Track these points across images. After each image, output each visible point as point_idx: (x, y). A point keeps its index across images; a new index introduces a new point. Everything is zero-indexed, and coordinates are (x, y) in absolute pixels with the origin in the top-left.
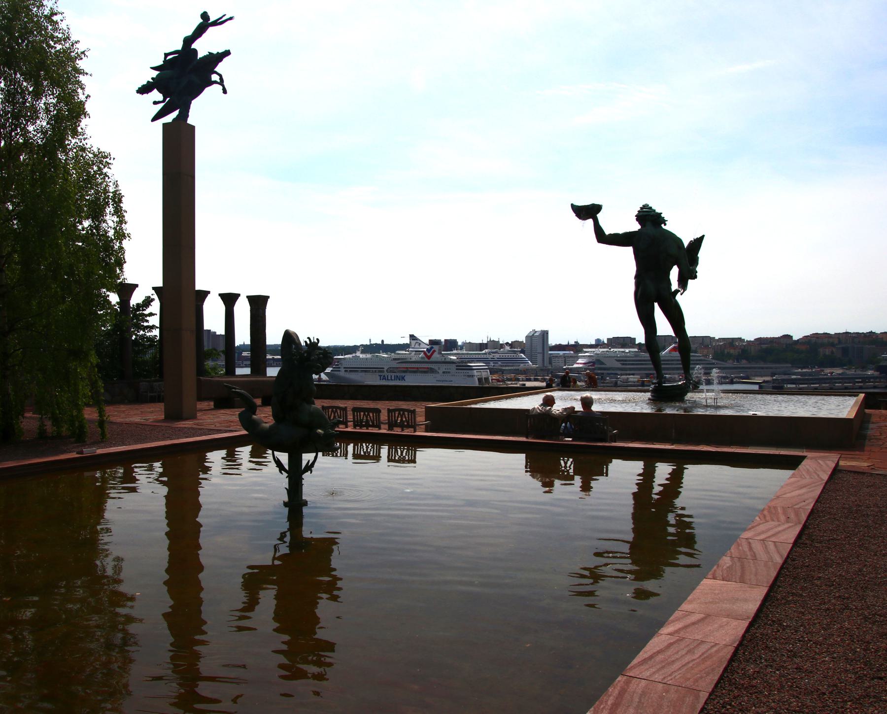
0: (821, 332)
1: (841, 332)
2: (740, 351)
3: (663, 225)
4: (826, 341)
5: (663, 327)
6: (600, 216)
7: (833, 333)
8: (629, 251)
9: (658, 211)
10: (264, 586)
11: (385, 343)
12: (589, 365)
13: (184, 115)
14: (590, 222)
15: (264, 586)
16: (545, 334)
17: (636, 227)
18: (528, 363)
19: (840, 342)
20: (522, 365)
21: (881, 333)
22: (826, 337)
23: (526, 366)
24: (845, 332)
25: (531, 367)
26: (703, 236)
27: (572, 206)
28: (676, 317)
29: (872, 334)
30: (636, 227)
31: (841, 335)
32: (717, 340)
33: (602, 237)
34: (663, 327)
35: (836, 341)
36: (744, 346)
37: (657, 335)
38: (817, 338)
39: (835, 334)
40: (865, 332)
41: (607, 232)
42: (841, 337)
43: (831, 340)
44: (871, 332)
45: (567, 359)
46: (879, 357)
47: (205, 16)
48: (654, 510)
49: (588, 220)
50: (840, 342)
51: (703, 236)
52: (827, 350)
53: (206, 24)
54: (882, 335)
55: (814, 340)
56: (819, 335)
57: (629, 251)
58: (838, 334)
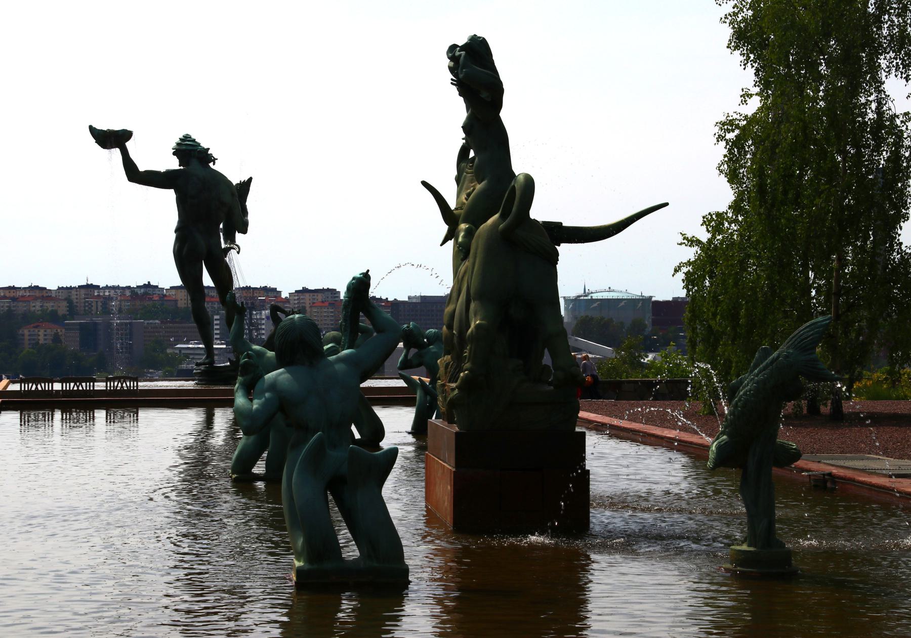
1: (75, 283)
3: (211, 164)
4: (36, 306)
6: (129, 145)
8: (170, 195)
9: (204, 145)
10: (387, 623)
14: (116, 152)
15: (387, 623)
17: (174, 164)
19: (72, 311)
21: (172, 288)
22: (36, 298)
24: (85, 284)
26: (250, 179)
28: (223, 275)
29: (150, 291)
30: (174, 164)
33: (134, 174)
35: (63, 309)
38: (14, 299)
39: (59, 288)
40: (133, 285)
41: (142, 168)
42: (74, 297)
43: (49, 305)
44: (148, 286)
46: (169, 351)
48: (556, 524)
49: (113, 150)
50: (72, 311)
51: (250, 179)
52: (42, 332)
54: (173, 292)
56: (21, 293)
57: (170, 195)
58: (67, 288)
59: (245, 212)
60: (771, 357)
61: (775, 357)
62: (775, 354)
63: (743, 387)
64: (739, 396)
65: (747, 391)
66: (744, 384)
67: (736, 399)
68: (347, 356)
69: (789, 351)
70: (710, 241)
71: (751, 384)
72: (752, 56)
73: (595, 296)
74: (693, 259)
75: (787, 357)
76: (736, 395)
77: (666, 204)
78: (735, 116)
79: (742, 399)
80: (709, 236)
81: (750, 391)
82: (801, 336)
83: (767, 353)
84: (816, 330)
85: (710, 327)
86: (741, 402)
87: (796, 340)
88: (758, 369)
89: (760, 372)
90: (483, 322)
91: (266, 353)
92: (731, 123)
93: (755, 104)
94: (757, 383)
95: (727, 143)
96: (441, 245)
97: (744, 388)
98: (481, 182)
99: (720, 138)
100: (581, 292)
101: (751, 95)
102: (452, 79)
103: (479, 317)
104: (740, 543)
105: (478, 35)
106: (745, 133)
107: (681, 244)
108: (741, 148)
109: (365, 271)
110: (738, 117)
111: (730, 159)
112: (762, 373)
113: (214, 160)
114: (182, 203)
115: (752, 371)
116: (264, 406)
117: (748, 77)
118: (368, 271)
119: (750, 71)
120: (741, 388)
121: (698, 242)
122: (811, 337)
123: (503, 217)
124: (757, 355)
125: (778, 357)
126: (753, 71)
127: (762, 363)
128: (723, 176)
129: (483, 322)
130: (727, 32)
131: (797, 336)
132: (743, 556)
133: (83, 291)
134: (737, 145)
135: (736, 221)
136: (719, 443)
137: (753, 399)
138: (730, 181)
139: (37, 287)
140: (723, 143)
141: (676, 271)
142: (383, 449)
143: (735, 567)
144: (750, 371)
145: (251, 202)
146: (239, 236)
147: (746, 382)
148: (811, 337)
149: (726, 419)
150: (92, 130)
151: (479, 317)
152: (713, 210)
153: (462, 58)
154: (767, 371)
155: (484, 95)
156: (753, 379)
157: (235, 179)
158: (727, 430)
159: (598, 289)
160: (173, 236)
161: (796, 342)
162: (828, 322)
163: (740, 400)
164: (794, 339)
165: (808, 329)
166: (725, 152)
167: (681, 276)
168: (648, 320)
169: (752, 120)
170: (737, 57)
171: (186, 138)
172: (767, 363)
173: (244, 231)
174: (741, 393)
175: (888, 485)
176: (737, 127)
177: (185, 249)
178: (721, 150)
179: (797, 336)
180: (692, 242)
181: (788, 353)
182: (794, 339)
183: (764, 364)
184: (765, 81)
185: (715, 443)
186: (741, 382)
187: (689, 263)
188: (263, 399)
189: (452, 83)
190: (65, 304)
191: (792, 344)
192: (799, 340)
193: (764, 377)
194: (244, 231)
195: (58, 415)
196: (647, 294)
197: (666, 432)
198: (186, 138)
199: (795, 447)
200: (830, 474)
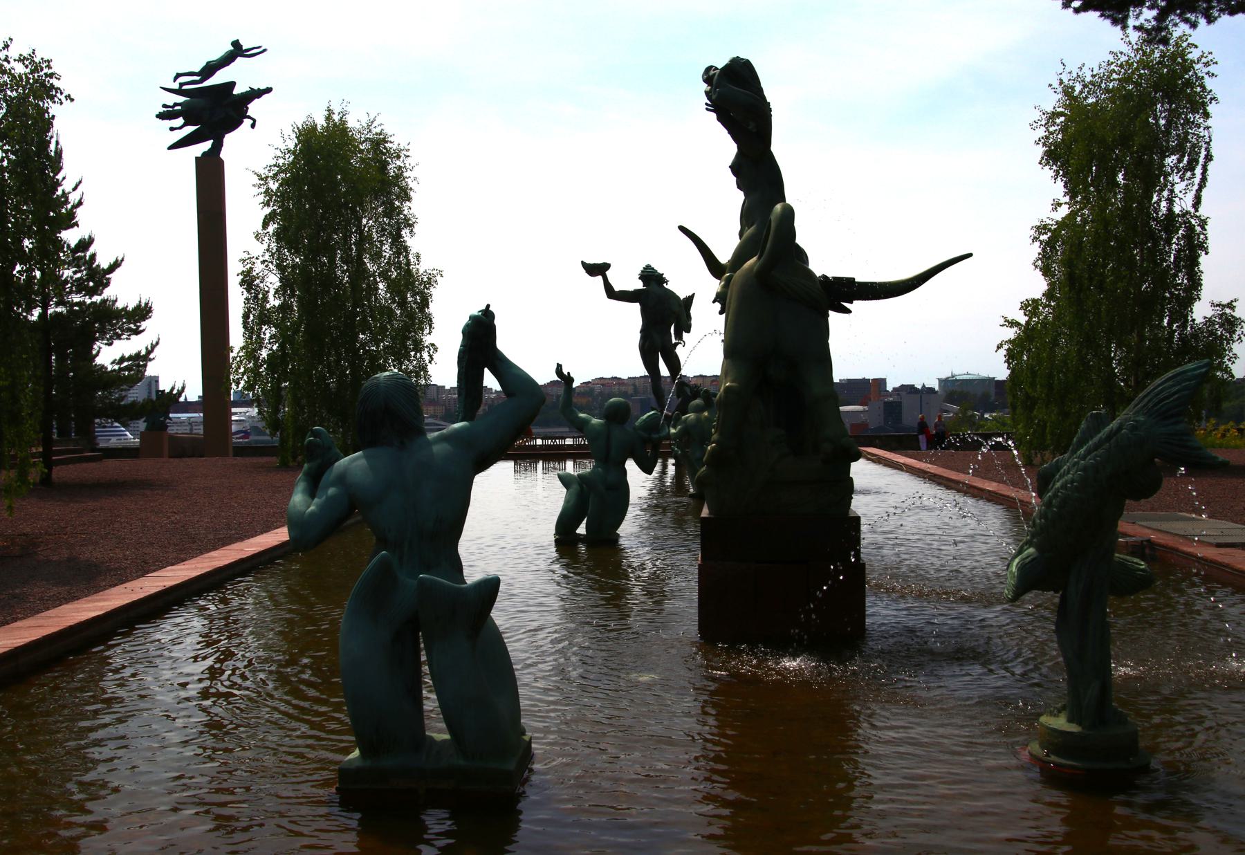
0: (608, 375)
2: (487, 408)
3: (665, 285)
5: (664, 371)
6: (608, 273)
7: (626, 378)
8: (636, 307)
9: (660, 271)
11: (188, 400)
12: (238, 436)
13: (217, 147)
14: (600, 278)
16: (153, 383)
17: (639, 285)
18: (126, 435)
20: (114, 440)
23: (123, 441)
25: (133, 442)
26: (694, 294)
27: (583, 263)
28: (674, 365)
30: (639, 285)
31: (637, 380)
32: (449, 390)
33: (611, 293)
34: (664, 371)
35: (630, 390)
36: (492, 400)
37: (838, 375)
41: (617, 289)
42: (637, 384)
43: (623, 388)
45: (194, 427)
47: (236, 44)
51: (694, 294)
53: (238, 51)
54: (695, 379)
55: (598, 388)
56: (607, 381)
57: (636, 307)
58: (633, 378)
59: (689, 317)
60: (1107, 429)
61: (1114, 429)
62: (1114, 424)
63: (1060, 476)
64: (1054, 489)
65: (1066, 482)
66: (1062, 471)
67: (1050, 494)
68: (457, 431)
69: (1137, 419)
70: (1028, 323)
71: (1074, 471)
72: (1061, 172)
73: (958, 378)
74: (1013, 338)
75: (1134, 428)
76: (1050, 487)
77: (970, 255)
78: (1049, 222)
79: (1060, 494)
80: (1027, 318)
81: (1072, 481)
82: (1157, 395)
83: (1099, 422)
84: (1184, 384)
85: (1027, 393)
86: (1058, 499)
87: (1149, 401)
88: (1085, 448)
89: (1088, 452)
90: (733, 384)
91: (590, 421)
92: (1045, 227)
93: (1064, 211)
94: (1085, 469)
95: (1041, 244)
96: (170, 148)
97: (1061, 477)
98: (751, 226)
99: (1035, 239)
100: (950, 375)
101: (1061, 204)
102: (706, 104)
103: (729, 379)
104: (1056, 712)
105: (741, 57)
106: (1055, 235)
107: (1003, 326)
108: (1053, 248)
109: (484, 308)
110: (1051, 222)
111: (1044, 256)
112: (1093, 454)
113: (667, 282)
114: (644, 312)
115: (1074, 451)
116: (322, 508)
117: (1058, 190)
118: (488, 306)
119: (1060, 184)
120: (1057, 476)
121: (1017, 324)
122: (1176, 396)
123: (759, 259)
124: (1083, 425)
125: (1120, 428)
126: (1063, 184)
127: (1092, 438)
128: (1038, 270)
129: (733, 384)
130: (1040, 150)
131: (1152, 394)
132: (1060, 740)
133: (642, 380)
134: (1050, 244)
135: (1049, 306)
136: (1023, 559)
137: (1076, 494)
138: (1045, 274)
139: (616, 378)
140: (1038, 244)
141: (998, 348)
142: (466, 583)
143: (1047, 755)
144: (1072, 451)
145: (694, 311)
146: (685, 334)
147: (1065, 467)
148: (1176, 396)
149: (1034, 522)
150: (583, 264)
151: (729, 379)
152: (1030, 297)
153: (716, 77)
154: (1100, 451)
155: (752, 126)
156: (1075, 464)
157: (682, 295)
158: (1035, 540)
159: (961, 373)
160: (639, 336)
161: (1151, 405)
162: (1204, 370)
163: (1055, 495)
164: (1146, 400)
165: (1170, 383)
166: (1040, 250)
167: (1003, 352)
168: (992, 391)
169: (1062, 224)
170: (1048, 172)
171: (648, 267)
172: (1101, 437)
173: (688, 331)
174: (1058, 485)
175: (1219, 559)
176: (1050, 230)
177: (647, 344)
178: (1036, 249)
179: (1152, 394)
180: (1013, 324)
181: (1136, 421)
182: (1146, 400)
183: (1096, 439)
184: (1071, 191)
185: (1017, 560)
186: (1057, 467)
187: (1010, 341)
188: (324, 498)
189: (707, 109)
190: (632, 387)
191: (1144, 406)
192: (1155, 400)
193: (1095, 460)
194: (688, 331)
195: (541, 463)
196: (991, 376)
197: (987, 484)
198: (648, 267)
199: (1143, 567)
200: (1149, 541)
